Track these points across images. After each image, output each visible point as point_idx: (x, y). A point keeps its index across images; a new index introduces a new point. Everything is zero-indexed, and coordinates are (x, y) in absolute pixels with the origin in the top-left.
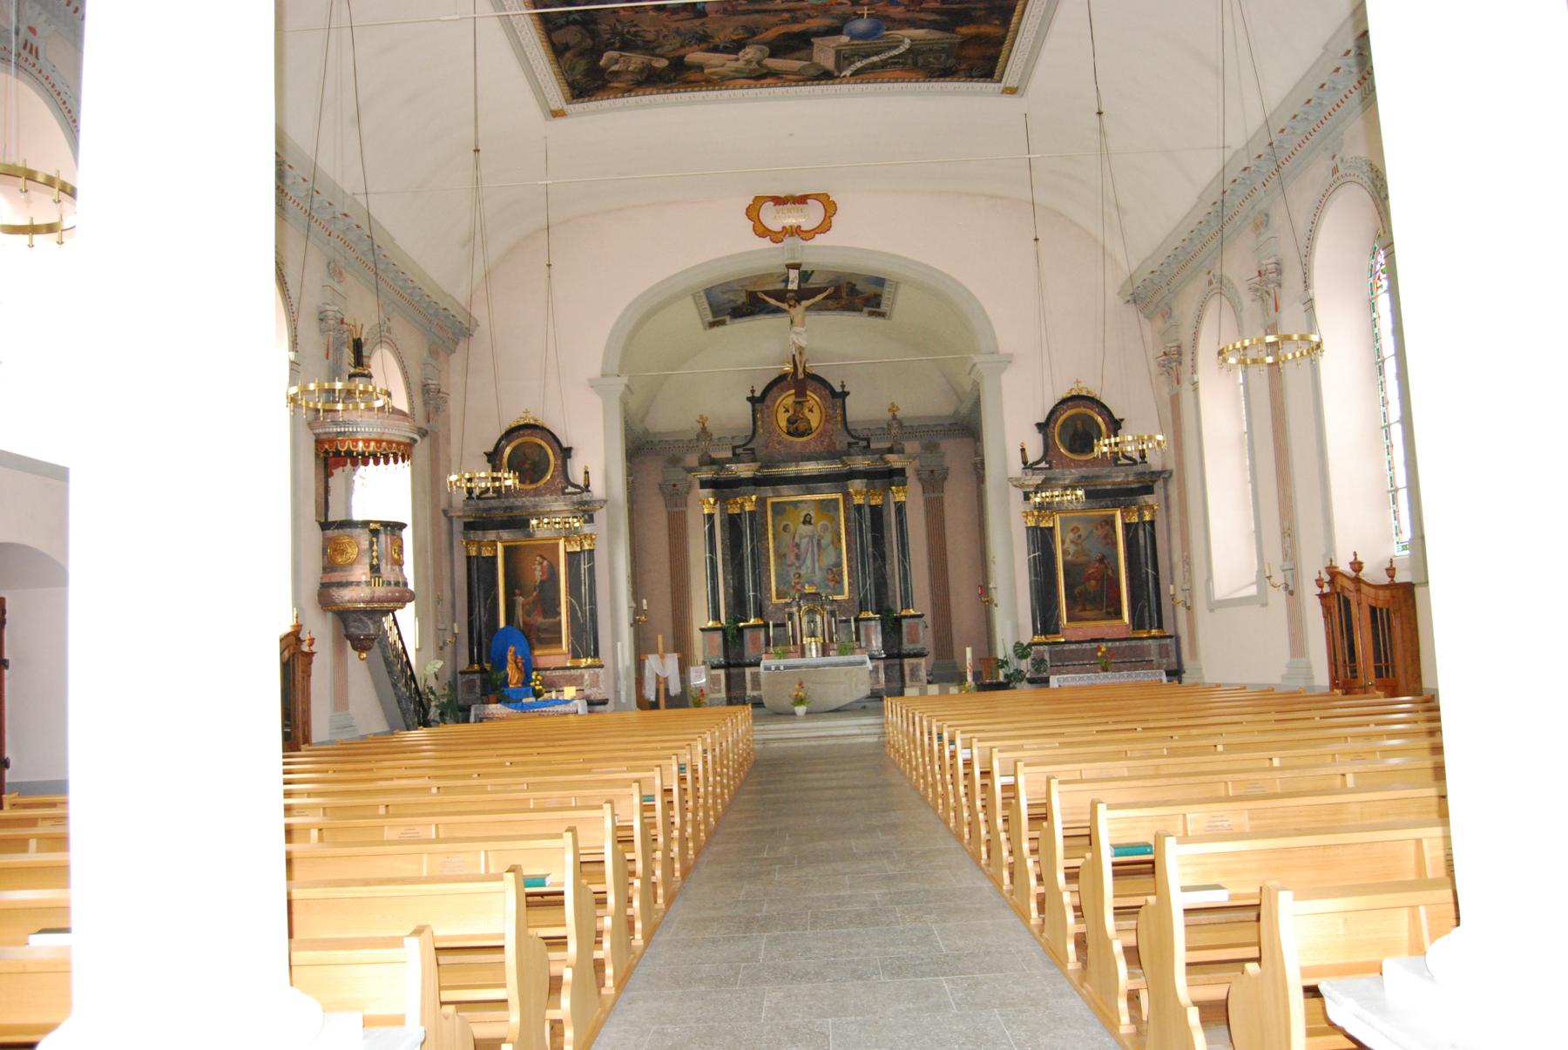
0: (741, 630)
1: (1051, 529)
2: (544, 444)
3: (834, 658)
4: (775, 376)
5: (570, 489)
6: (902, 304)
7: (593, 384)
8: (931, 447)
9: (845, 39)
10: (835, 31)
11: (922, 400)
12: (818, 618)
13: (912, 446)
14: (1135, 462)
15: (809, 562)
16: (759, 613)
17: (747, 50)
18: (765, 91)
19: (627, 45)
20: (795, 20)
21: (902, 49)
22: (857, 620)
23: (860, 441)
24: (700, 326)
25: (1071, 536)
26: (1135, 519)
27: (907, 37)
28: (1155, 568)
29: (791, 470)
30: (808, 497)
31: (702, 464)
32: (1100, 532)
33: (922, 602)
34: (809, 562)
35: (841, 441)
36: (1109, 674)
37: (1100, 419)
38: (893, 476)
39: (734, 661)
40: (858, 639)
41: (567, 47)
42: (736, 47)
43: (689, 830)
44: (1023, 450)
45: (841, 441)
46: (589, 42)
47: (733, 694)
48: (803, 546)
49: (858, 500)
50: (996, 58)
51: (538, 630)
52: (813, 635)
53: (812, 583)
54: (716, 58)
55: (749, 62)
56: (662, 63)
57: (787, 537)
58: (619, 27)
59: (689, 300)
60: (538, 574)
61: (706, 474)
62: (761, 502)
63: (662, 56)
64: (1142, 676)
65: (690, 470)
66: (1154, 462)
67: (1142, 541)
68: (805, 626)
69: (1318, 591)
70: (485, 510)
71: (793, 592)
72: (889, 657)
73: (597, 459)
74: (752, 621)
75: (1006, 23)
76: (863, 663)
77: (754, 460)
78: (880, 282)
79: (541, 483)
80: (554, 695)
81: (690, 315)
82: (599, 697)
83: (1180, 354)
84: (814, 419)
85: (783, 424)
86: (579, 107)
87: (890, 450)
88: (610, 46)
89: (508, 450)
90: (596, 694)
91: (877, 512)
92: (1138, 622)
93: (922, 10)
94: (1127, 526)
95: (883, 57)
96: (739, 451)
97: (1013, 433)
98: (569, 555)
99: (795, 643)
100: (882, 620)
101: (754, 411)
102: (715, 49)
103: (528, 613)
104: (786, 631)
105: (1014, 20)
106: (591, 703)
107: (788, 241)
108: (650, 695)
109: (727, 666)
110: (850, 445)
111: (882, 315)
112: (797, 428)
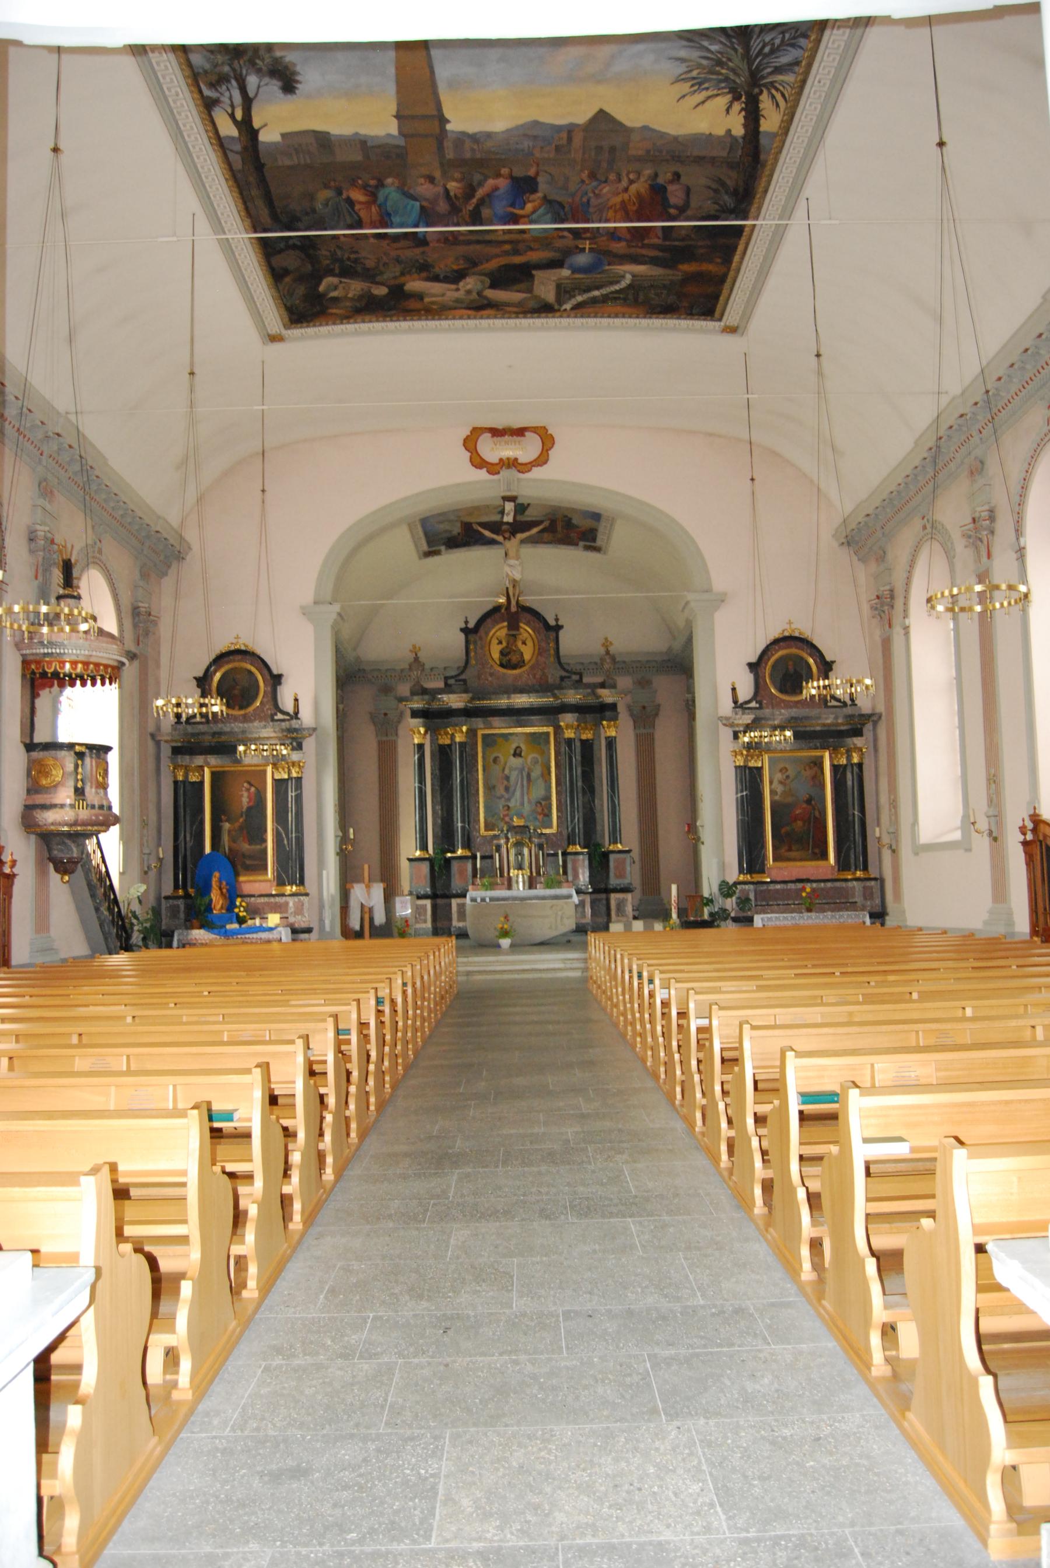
0: (448, 861)
1: (760, 769)
2: (253, 669)
3: (540, 891)
4: (489, 607)
5: (279, 716)
6: (618, 540)
7: (305, 612)
8: (643, 683)
9: (566, 272)
10: (556, 264)
11: (635, 637)
12: (526, 851)
13: (624, 682)
14: (845, 704)
15: (518, 793)
16: (467, 844)
18: (485, 322)
19: (347, 272)
20: (516, 252)
21: (623, 284)
22: (564, 854)
23: (572, 675)
24: (414, 555)
25: (779, 776)
26: (843, 761)
27: (628, 272)
28: (862, 810)
29: (503, 702)
30: (519, 730)
31: (413, 693)
32: (809, 773)
33: (630, 837)
34: (518, 793)
35: (554, 674)
36: (813, 915)
37: (811, 661)
38: (604, 711)
39: (440, 890)
40: (565, 873)
41: (286, 272)
42: (456, 277)
43: (418, 1023)
44: (734, 689)
45: (554, 674)
46: (309, 267)
47: (439, 925)
48: (512, 779)
49: (569, 734)
50: (717, 297)
51: (244, 856)
52: (520, 867)
53: (520, 816)
54: (436, 288)
55: (469, 292)
56: (381, 291)
57: (496, 769)
58: (339, 253)
60: (245, 800)
61: (417, 704)
62: (472, 733)
64: (847, 917)
65: (401, 700)
66: (865, 705)
67: (849, 783)
68: (512, 858)
69: (1021, 838)
70: (193, 735)
71: (502, 824)
72: (596, 891)
73: (307, 686)
74: (460, 852)
76: (570, 897)
77: (466, 691)
78: (597, 517)
79: (251, 709)
80: (258, 922)
81: (404, 545)
82: (304, 925)
83: (892, 597)
85: (496, 655)
87: (603, 685)
88: (330, 272)
90: (301, 922)
91: (587, 747)
92: (843, 864)
93: (643, 246)
94: (835, 768)
95: (604, 291)
96: (451, 682)
97: (725, 671)
98: (279, 783)
99: (502, 875)
100: (589, 853)
101: (467, 642)
102: (436, 279)
103: (233, 840)
104: (493, 864)
105: (736, 258)
106: (295, 931)
107: (505, 473)
108: (355, 924)
109: (433, 897)
110: (562, 679)
111: (597, 549)
112: (510, 660)
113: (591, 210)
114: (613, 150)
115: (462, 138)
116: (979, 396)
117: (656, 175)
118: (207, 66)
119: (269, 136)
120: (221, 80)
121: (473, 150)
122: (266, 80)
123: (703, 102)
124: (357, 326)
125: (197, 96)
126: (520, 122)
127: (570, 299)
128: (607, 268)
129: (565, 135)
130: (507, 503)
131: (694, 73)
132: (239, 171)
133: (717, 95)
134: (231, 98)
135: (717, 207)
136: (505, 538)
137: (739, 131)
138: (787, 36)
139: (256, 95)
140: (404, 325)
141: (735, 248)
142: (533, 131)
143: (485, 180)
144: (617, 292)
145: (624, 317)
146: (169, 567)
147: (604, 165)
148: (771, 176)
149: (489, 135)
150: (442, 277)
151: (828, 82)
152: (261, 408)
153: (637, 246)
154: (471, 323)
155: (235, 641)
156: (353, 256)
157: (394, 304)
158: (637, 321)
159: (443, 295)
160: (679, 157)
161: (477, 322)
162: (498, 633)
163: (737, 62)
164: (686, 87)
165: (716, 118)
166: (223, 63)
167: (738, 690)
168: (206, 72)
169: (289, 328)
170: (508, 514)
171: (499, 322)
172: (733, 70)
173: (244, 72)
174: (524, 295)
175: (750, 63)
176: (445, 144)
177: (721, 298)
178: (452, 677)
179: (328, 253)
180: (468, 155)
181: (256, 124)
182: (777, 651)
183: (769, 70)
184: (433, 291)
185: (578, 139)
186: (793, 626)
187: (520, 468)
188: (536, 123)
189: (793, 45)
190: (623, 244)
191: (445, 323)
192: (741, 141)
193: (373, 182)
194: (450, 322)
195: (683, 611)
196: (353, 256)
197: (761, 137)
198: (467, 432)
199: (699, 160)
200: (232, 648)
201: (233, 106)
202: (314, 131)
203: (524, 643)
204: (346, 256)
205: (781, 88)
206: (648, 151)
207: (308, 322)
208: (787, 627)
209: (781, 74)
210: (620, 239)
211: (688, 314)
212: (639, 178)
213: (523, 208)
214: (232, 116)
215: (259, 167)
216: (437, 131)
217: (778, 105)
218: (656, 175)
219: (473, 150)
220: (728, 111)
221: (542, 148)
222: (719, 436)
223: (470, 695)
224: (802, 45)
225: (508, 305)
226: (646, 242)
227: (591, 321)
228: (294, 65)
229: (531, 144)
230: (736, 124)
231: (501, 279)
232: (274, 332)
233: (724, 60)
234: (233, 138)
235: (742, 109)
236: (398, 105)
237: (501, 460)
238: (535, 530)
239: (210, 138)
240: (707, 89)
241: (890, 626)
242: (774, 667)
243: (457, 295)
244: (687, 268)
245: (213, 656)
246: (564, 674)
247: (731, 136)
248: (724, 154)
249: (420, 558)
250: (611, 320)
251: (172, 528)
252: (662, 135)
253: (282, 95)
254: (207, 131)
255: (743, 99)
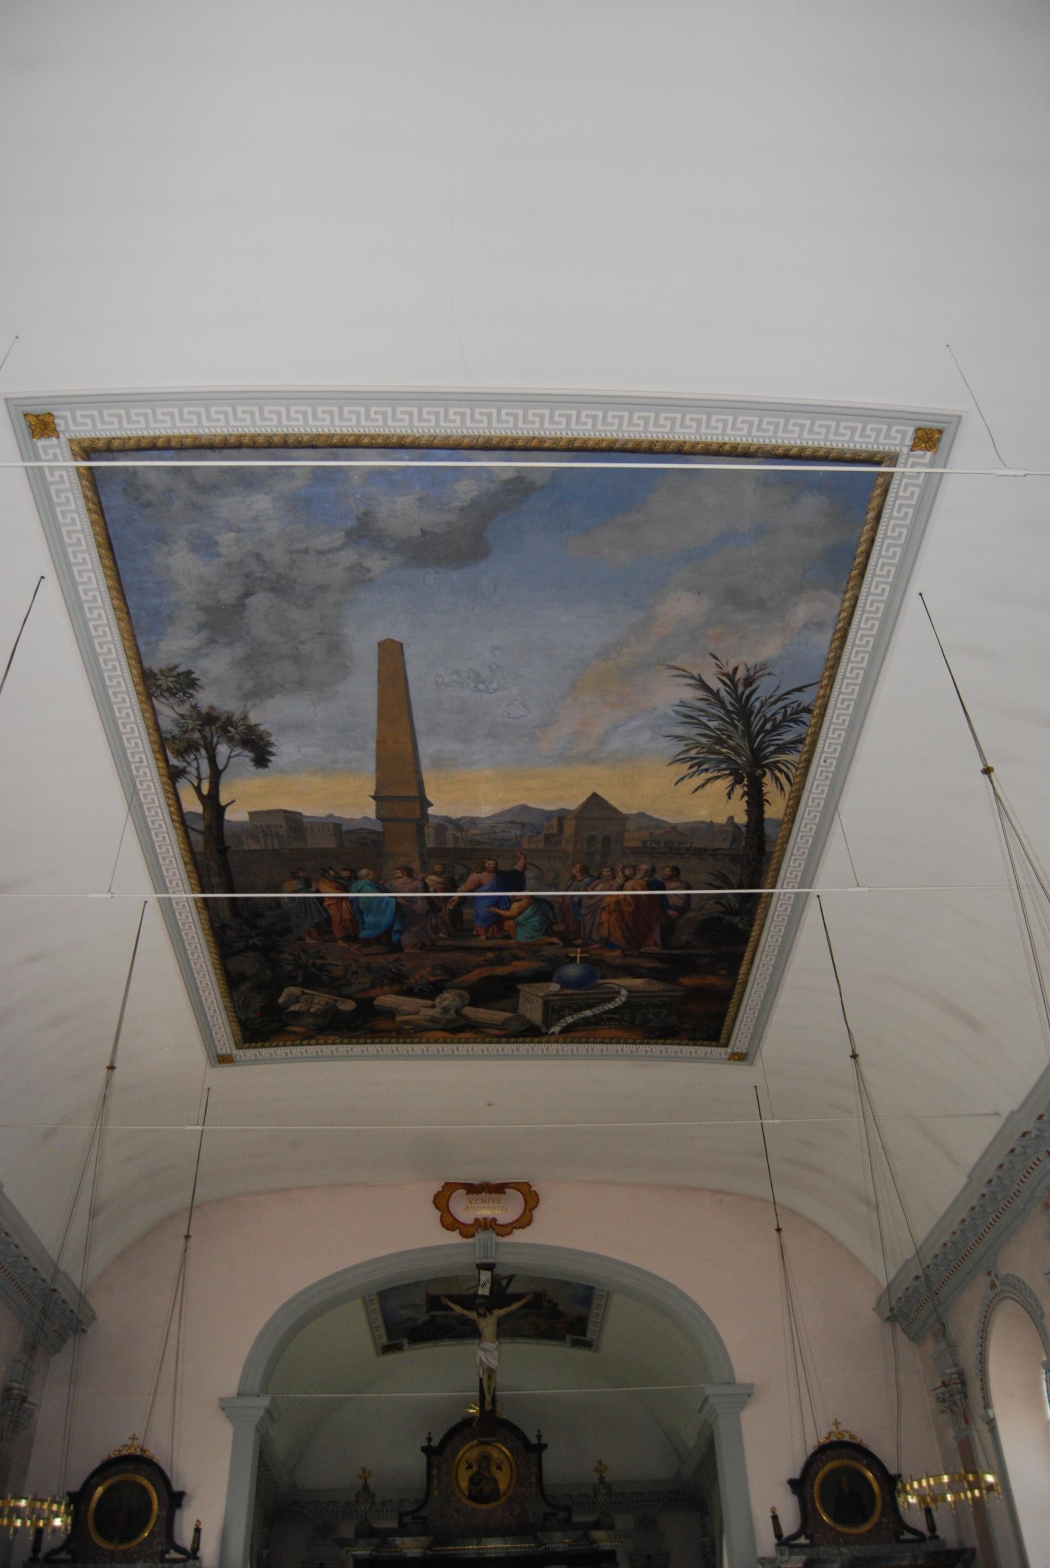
2: (146, 1483)
4: (458, 1420)
5: (174, 1555)
6: (615, 1326)
7: (225, 1406)
9: (554, 987)
10: (542, 977)
11: (635, 1460)
13: (624, 1521)
14: (922, 1537)
17: (446, 995)
18: (463, 1048)
19: (312, 980)
20: (500, 962)
21: (618, 1002)
27: (625, 986)
31: (359, 1535)
37: (870, 1475)
41: (243, 978)
42: (431, 991)
46: (269, 973)
50: (722, 1017)
54: (408, 1003)
55: (446, 1010)
56: (348, 1006)
58: (303, 957)
59: (358, 1303)
63: (349, 997)
65: (342, 1543)
75: (734, 973)
78: (591, 1288)
81: (355, 1330)
83: (963, 1382)
84: (503, 1480)
85: (464, 1484)
86: (250, 1053)
87: (597, 1526)
88: (291, 980)
89: (100, 1490)
93: (643, 955)
95: (597, 1011)
96: (407, 1519)
102: (409, 992)
105: (743, 970)
107: (481, 1236)
111: (587, 1345)
112: (482, 1489)
113: (583, 911)
114: (606, 840)
115: (446, 824)
116: (1030, 1125)
117: (654, 870)
118: (176, 732)
119: (236, 815)
120: (191, 747)
121: (456, 838)
122: (238, 750)
123: (703, 785)
124: (318, 1048)
125: (162, 764)
126: (508, 806)
127: (558, 1020)
128: (600, 981)
129: (554, 822)
130: (483, 1272)
131: (693, 753)
132: (200, 853)
133: (718, 777)
134: (198, 769)
135: (720, 908)
136: (479, 1315)
137: (742, 819)
138: (789, 710)
139: (225, 767)
140: (372, 1048)
141: (741, 958)
142: (521, 818)
143: (469, 874)
144: (610, 1011)
145: (618, 1043)
146: (64, 1341)
147: (598, 858)
148: (778, 870)
149: (474, 821)
150: (416, 990)
151: (835, 762)
152: (200, 1128)
153: (632, 956)
154: (448, 1048)
155: (129, 1442)
156: (319, 962)
157: (360, 1024)
158: (634, 1047)
159: (417, 1013)
160: (678, 849)
161: (454, 1046)
162: (468, 1455)
163: (737, 740)
164: (684, 769)
165: (713, 804)
166: (193, 729)
167: (781, 1519)
168: (174, 737)
169: (241, 1048)
170: (484, 1286)
171: (479, 1048)
172: (733, 749)
173: (215, 740)
174: (508, 1015)
175: (751, 742)
176: (426, 830)
177: (727, 1019)
178: (407, 1514)
179: (291, 958)
180: (450, 845)
181: (223, 800)
182: (824, 1464)
183: (772, 749)
184: (405, 1008)
185: (569, 829)
186: (841, 1428)
187: (500, 1230)
188: (524, 808)
189: (796, 721)
190: (617, 953)
191: (418, 1048)
192: (744, 829)
193: (345, 874)
194: (424, 1047)
195: (700, 1411)
196: (319, 962)
197: (766, 824)
198: (438, 1187)
199: (700, 852)
200: (125, 1452)
201: (200, 779)
202: (285, 812)
203: (499, 1468)
204: (311, 962)
205: (785, 769)
206: (645, 842)
207: (264, 1041)
208: (834, 1428)
209: (783, 753)
210: (614, 947)
211: (690, 1039)
212: (635, 874)
213: (508, 909)
214: (198, 789)
215: (222, 849)
216: (418, 814)
217: (782, 789)
218: (654, 870)
219: (456, 838)
220: (729, 795)
221: (531, 837)
222: (729, 1194)
223: (431, 1538)
224: (804, 720)
225: (488, 1026)
226: (643, 950)
227: (583, 1048)
228: (269, 734)
229: (518, 833)
230: (738, 810)
231: (480, 995)
232: (223, 1052)
233: (724, 737)
234: (197, 814)
235: (745, 794)
236: (378, 784)
237: (477, 1220)
238: (516, 1306)
239: (171, 813)
240: (707, 770)
241: (967, 1422)
242: (823, 1485)
243: (431, 1012)
244: (688, 981)
245: (96, 1463)
246: (549, 1510)
247: (733, 824)
248: (726, 845)
249: (378, 1355)
250: (604, 1047)
251: (74, 1287)
252: (660, 824)
253: (253, 769)
254: (169, 805)
255: (745, 782)
